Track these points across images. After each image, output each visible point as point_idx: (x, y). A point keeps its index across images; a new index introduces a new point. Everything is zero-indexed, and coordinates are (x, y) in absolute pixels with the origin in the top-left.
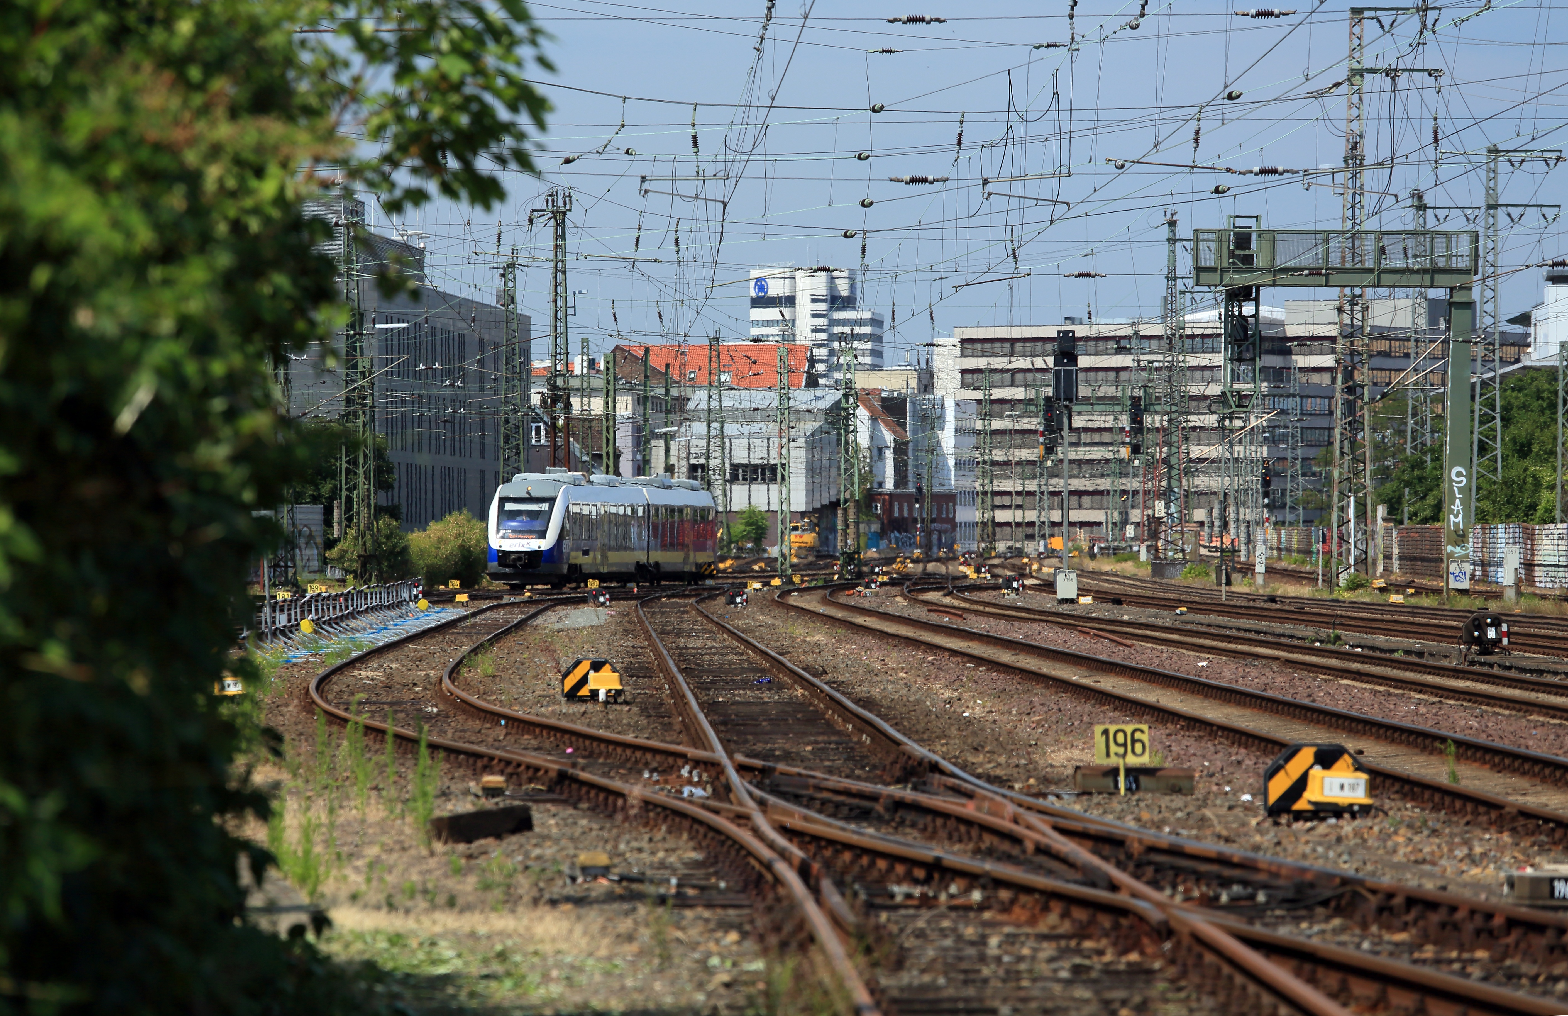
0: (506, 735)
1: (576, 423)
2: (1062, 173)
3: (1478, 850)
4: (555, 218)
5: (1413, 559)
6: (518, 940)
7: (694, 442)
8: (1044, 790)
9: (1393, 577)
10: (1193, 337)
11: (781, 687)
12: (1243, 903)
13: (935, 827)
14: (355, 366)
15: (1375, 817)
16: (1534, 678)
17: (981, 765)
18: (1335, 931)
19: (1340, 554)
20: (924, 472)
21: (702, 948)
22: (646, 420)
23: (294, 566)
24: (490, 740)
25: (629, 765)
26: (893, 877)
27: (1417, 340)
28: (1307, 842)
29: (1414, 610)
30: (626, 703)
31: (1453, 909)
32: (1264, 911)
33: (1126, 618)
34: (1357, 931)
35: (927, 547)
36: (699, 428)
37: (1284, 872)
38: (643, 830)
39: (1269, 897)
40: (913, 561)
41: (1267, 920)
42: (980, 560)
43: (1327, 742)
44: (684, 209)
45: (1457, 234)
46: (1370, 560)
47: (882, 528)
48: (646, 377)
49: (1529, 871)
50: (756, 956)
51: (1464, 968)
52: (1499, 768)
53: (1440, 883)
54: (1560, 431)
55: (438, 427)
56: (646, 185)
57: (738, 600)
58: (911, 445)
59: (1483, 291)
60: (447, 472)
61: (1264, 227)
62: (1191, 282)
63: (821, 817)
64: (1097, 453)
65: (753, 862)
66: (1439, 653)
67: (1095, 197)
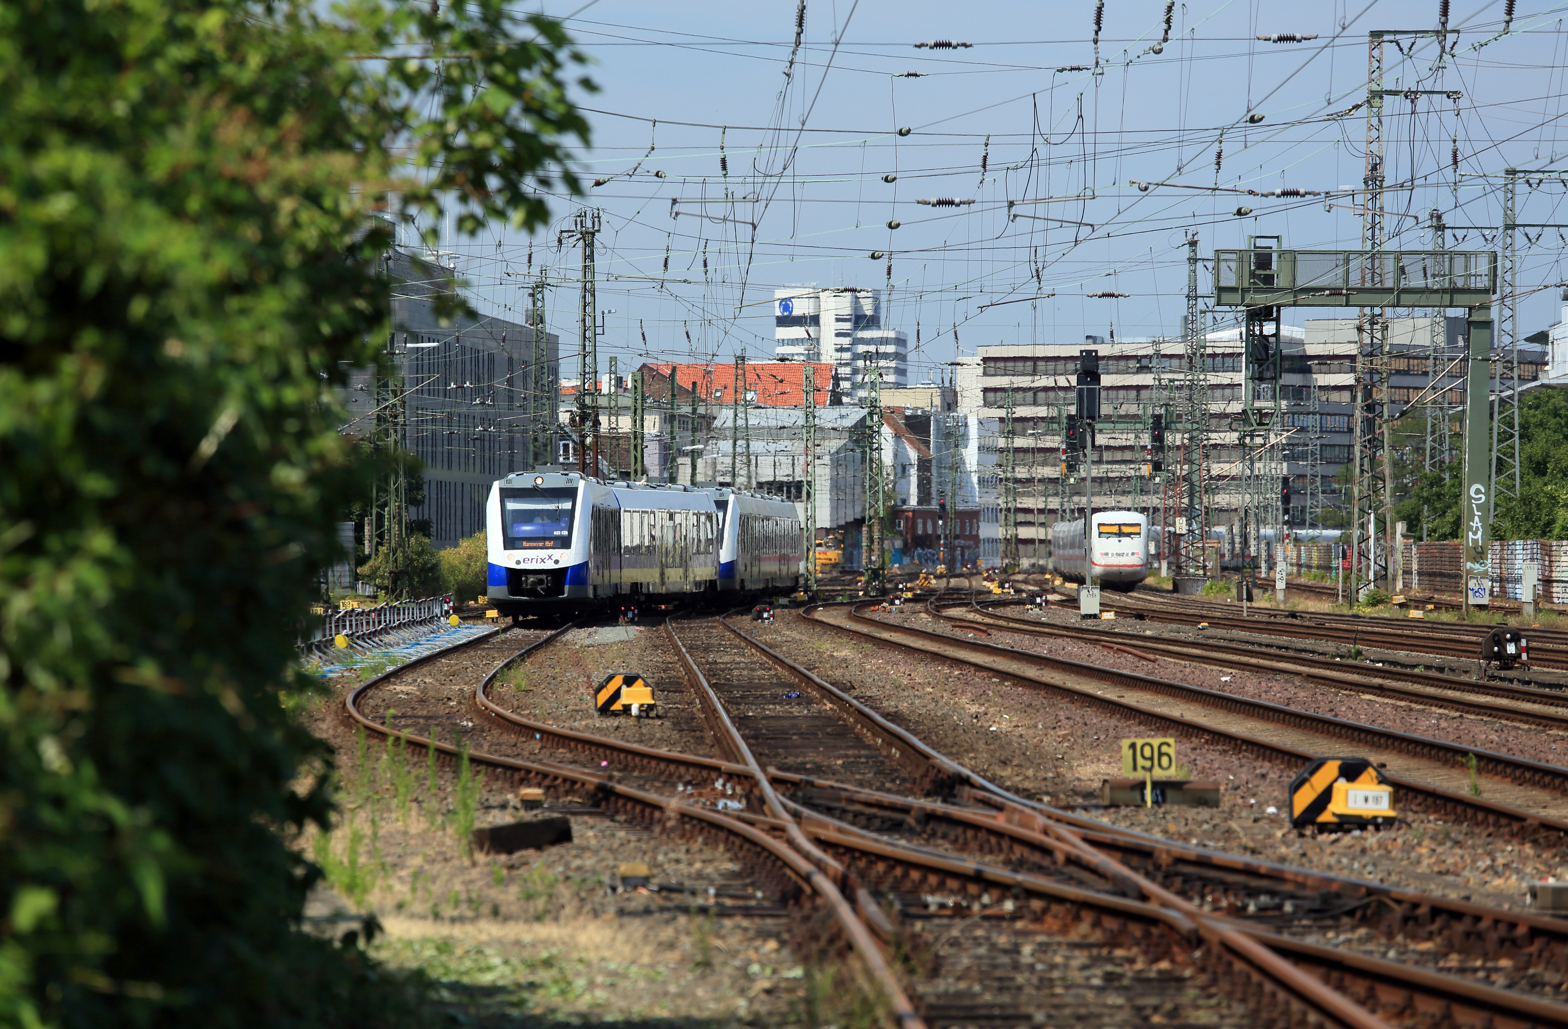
0: (541, 748)
1: (604, 441)
2: (1088, 195)
3: (1500, 861)
4: (583, 238)
5: (1430, 574)
7: (720, 459)
9: (1412, 593)
10: (1214, 356)
11: (810, 702)
12: (1271, 913)
13: (966, 839)
14: (386, 385)
15: (1399, 829)
17: (1009, 778)
18: (1361, 941)
19: (1360, 570)
20: (949, 488)
21: (742, 956)
22: (673, 438)
23: (327, 583)
24: (526, 753)
25: (663, 778)
26: (926, 887)
27: (1435, 359)
28: (1332, 854)
29: (1435, 626)
30: (658, 717)
31: (1478, 919)
32: (1292, 921)
33: (1148, 633)
34: (1383, 940)
35: (951, 564)
36: (726, 446)
37: (1310, 882)
38: (680, 842)
39: (1296, 907)
40: (936, 577)
41: (1294, 930)
42: (1003, 577)
43: (1350, 755)
44: (712, 230)
45: (1476, 254)
46: (1390, 576)
47: (906, 544)
48: (673, 395)
49: (1551, 881)
50: (795, 964)
51: (1488, 977)
53: (1463, 893)
55: (467, 444)
56: (676, 208)
57: (765, 615)
58: (934, 462)
59: (1501, 311)
61: (1285, 246)
62: (1211, 302)
63: (854, 829)
64: (1117, 471)
65: (789, 872)
66: (1459, 668)
67: (1119, 219)
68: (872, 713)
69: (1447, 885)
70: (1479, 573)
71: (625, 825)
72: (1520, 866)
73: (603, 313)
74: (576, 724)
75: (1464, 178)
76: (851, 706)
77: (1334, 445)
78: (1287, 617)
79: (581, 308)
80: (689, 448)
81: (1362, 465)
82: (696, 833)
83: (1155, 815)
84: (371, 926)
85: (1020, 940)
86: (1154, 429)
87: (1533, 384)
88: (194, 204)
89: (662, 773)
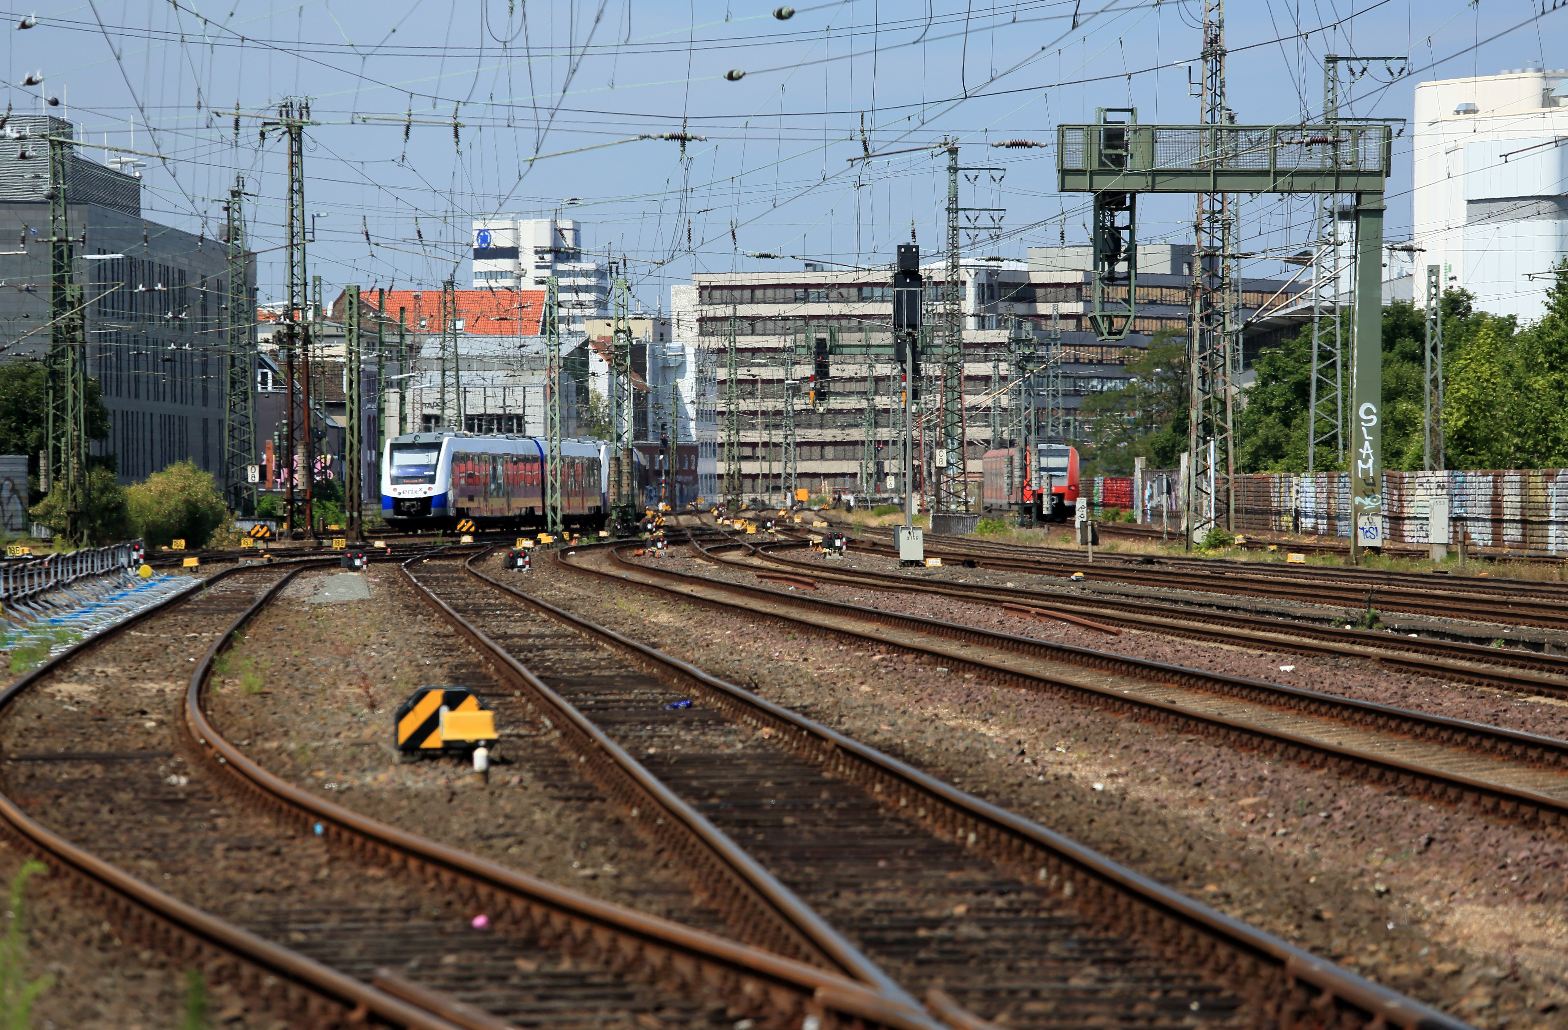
5: (1247, 512)
33: (1010, 585)
60: (167, 420)
61: (1143, 119)
70: (1371, 510)
78: (1143, 562)
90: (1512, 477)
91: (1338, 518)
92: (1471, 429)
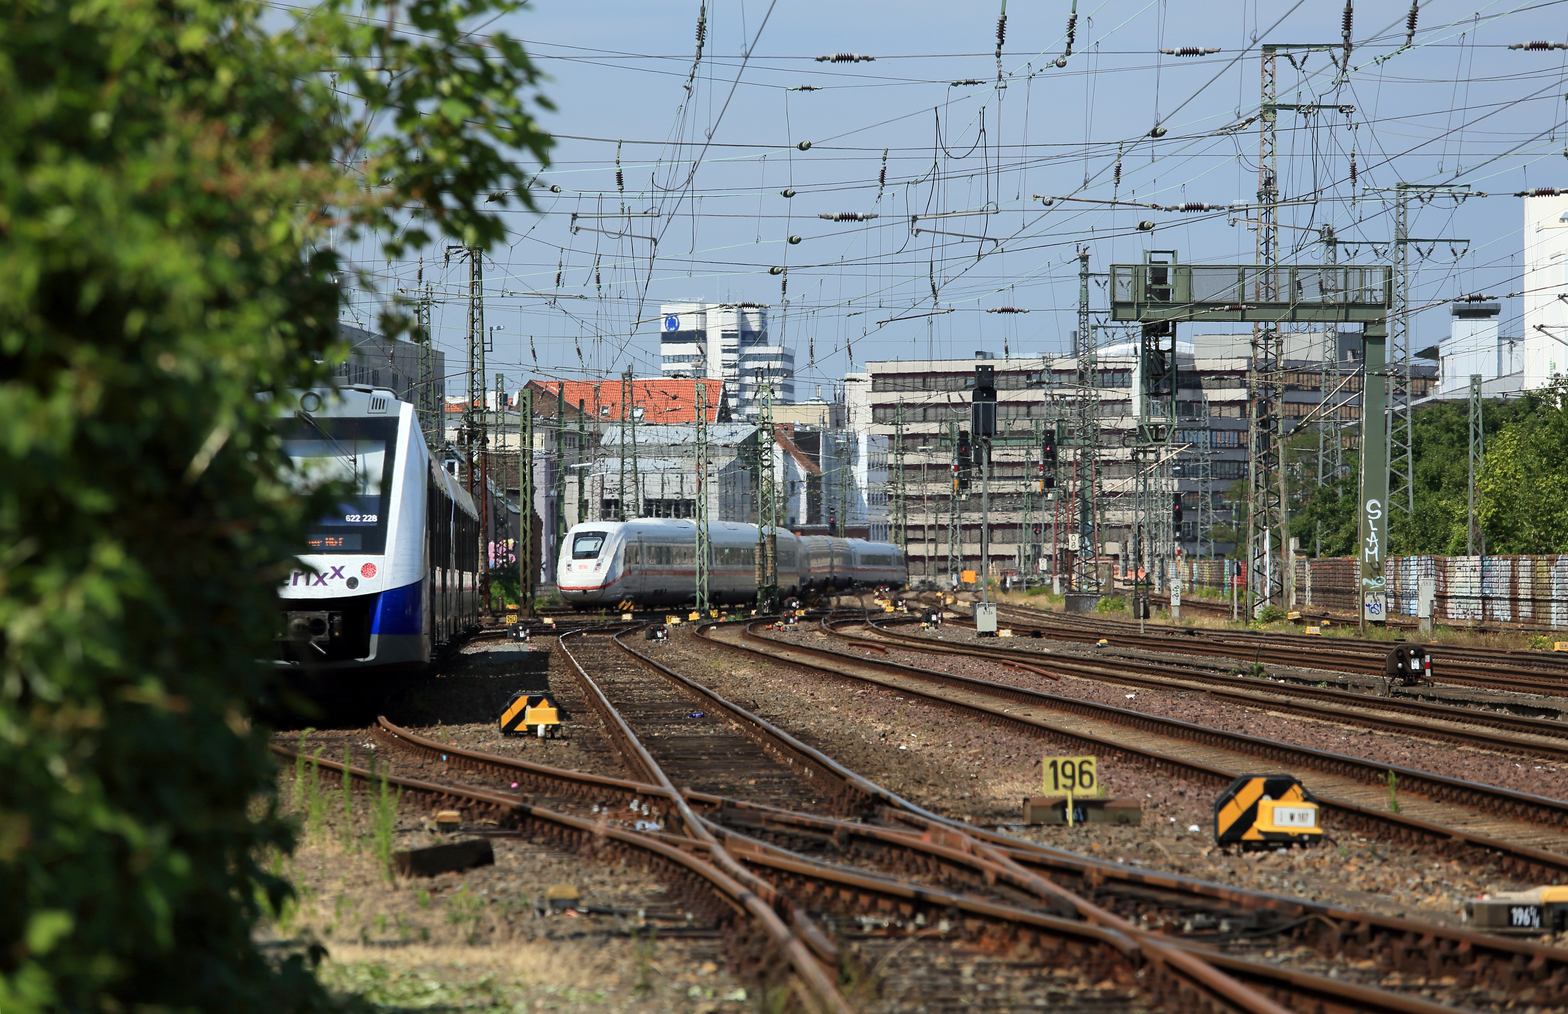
0: (449, 770)
3: (1429, 879)
6: (496, 971)
7: (608, 477)
8: (993, 822)
10: (1105, 371)
11: (714, 721)
12: (1207, 932)
13: (891, 858)
16: (1459, 708)
17: (926, 798)
20: (838, 506)
21: (680, 978)
22: (561, 456)
24: (433, 775)
25: (576, 800)
26: (858, 908)
30: (564, 738)
31: (1419, 936)
32: (1228, 940)
33: (1046, 650)
34: (1323, 959)
36: (614, 463)
37: (1245, 901)
39: (1232, 925)
44: (608, 246)
45: (1371, 268)
46: (1285, 592)
49: (1486, 898)
50: (737, 986)
52: (1437, 798)
53: (1397, 911)
54: (1472, 463)
58: (823, 479)
59: (1393, 326)
61: (1181, 261)
64: (1010, 487)
65: (718, 894)
66: (1362, 685)
68: (781, 732)
69: (1379, 903)
70: (1376, 589)
71: (543, 847)
72: (1450, 883)
73: (491, 329)
74: (481, 745)
75: (1367, 192)
76: (758, 725)
77: (1225, 461)
78: (1185, 633)
79: (469, 324)
80: (577, 466)
81: (1257, 481)
82: (618, 854)
83: (1077, 833)
84: (318, 952)
85: (959, 961)
86: (1045, 446)
87: (1424, 400)
88: (175, 218)
89: (574, 794)
90: (1525, 562)
91: (1402, 597)
92: (1501, 519)
